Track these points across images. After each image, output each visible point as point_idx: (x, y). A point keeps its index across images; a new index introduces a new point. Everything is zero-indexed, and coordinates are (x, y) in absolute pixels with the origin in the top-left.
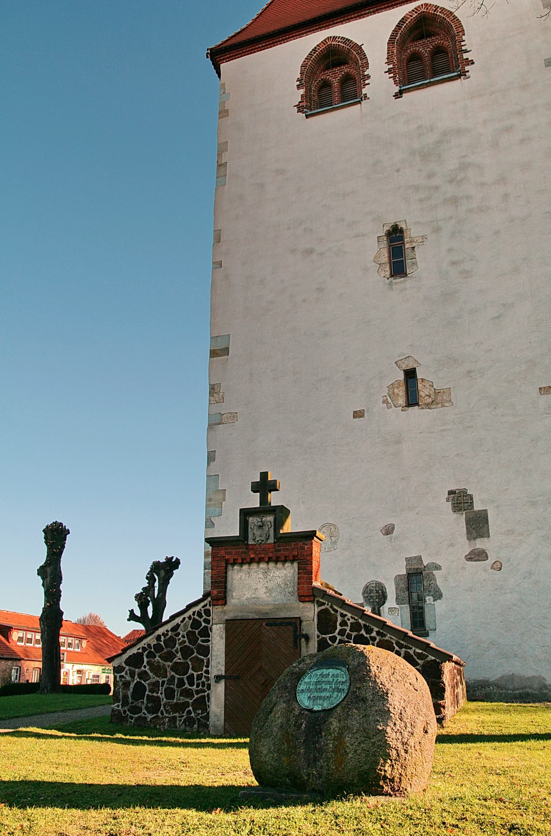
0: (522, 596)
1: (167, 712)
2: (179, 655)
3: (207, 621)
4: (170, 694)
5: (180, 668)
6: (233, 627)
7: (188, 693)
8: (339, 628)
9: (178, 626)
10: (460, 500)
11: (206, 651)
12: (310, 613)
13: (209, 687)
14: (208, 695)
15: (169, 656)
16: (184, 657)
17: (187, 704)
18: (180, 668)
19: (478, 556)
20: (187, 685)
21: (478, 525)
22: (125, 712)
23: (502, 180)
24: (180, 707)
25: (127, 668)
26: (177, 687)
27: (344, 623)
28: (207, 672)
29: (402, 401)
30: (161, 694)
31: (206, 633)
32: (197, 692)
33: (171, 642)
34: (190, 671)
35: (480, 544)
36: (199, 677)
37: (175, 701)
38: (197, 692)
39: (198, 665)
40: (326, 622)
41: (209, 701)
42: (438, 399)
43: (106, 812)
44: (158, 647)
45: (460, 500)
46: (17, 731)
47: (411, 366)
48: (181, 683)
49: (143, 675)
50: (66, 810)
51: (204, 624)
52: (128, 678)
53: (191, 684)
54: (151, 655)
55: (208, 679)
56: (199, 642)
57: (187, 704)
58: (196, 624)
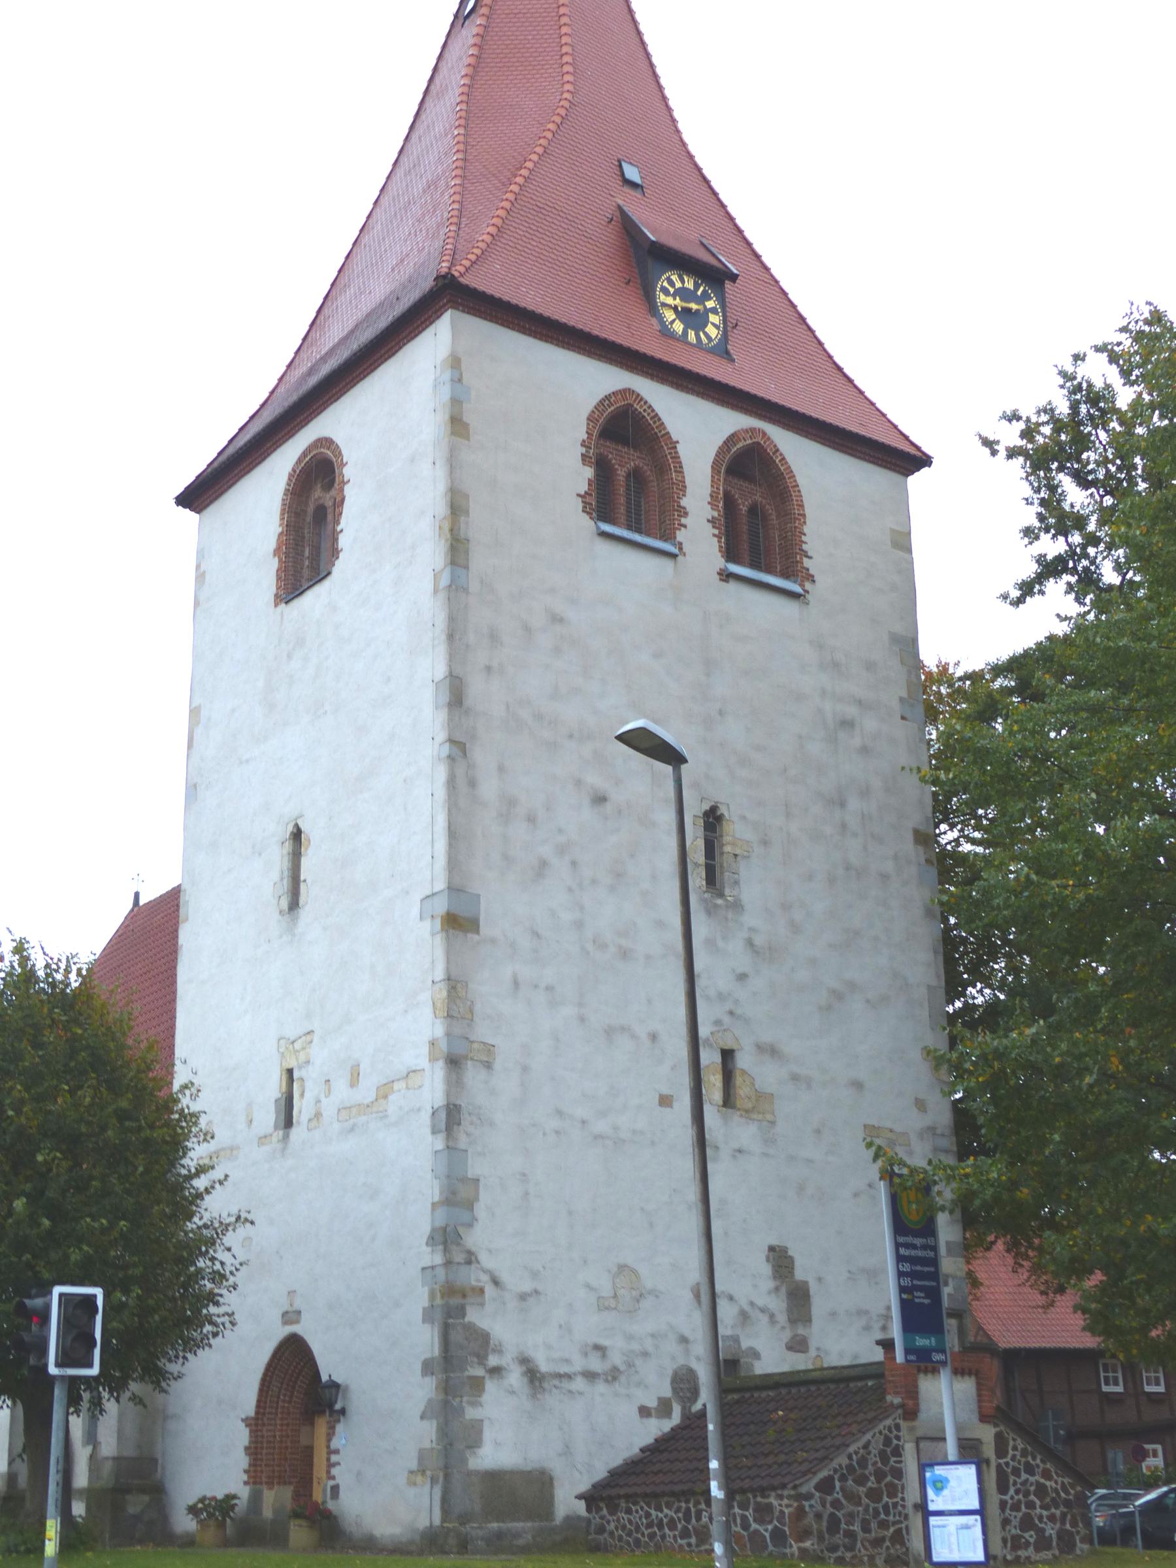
1: (866, 1549)
2: (872, 1478)
3: (898, 1438)
4: (866, 1529)
5: (874, 1495)
7: (884, 1525)
8: (1011, 1452)
9: (869, 1442)
11: (898, 1474)
13: (906, 1517)
14: (907, 1528)
16: (879, 1481)
17: (883, 1539)
18: (874, 1495)
20: (883, 1516)
22: (822, 1551)
24: (878, 1542)
25: (817, 1494)
26: (887, 1503)
27: (1015, 1448)
28: (903, 1499)
30: (856, 1527)
31: (897, 1452)
32: (894, 1523)
33: (863, 1462)
34: (885, 1499)
35: (801, 1331)
36: (895, 1505)
37: (873, 1534)
38: (894, 1523)
39: (893, 1491)
41: (908, 1533)
43: (47, 1542)
44: (850, 1468)
46: (656, 722)
48: (877, 1513)
49: (836, 1504)
51: (895, 1442)
52: (820, 1508)
53: (887, 1513)
54: (843, 1478)
55: (904, 1506)
56: (892, 1462)
57: (883, 1539)
58: (887, 1441)
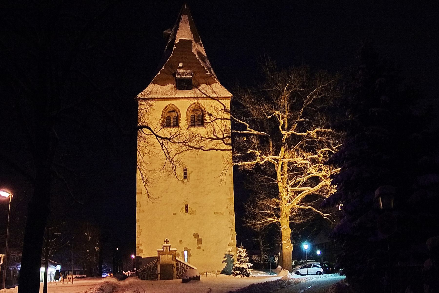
0: (277, 201)
4: (150, 277)
6: (161, 266)
10: (196, 236)
12: (175, 263)
15: (150, 270)
19: (199, 248)
21: (199, 241)
23: (211, 159)
29: (184, 212)
31: (157, 266)
33: (150, 268)
35: (199, 246)
39: (155, 272)
40: (177, 265)
42: (193, 212)
45: (196, 236)
47: (187, 204)
50: (288, 221)
58: (155, 265)
